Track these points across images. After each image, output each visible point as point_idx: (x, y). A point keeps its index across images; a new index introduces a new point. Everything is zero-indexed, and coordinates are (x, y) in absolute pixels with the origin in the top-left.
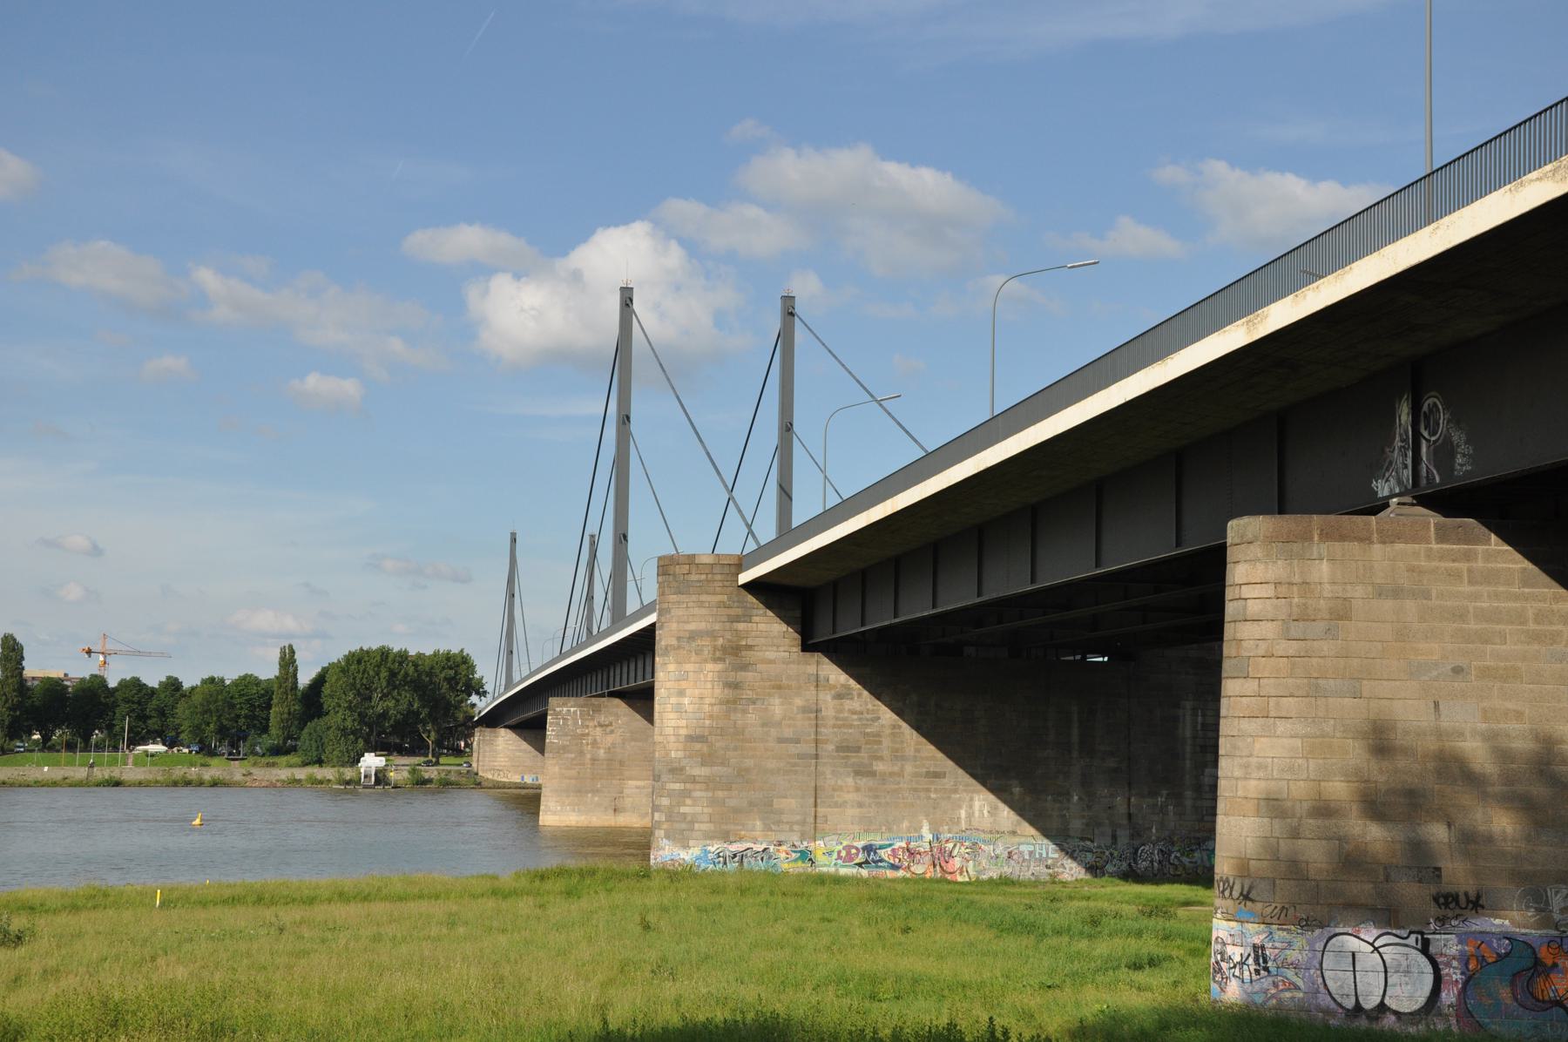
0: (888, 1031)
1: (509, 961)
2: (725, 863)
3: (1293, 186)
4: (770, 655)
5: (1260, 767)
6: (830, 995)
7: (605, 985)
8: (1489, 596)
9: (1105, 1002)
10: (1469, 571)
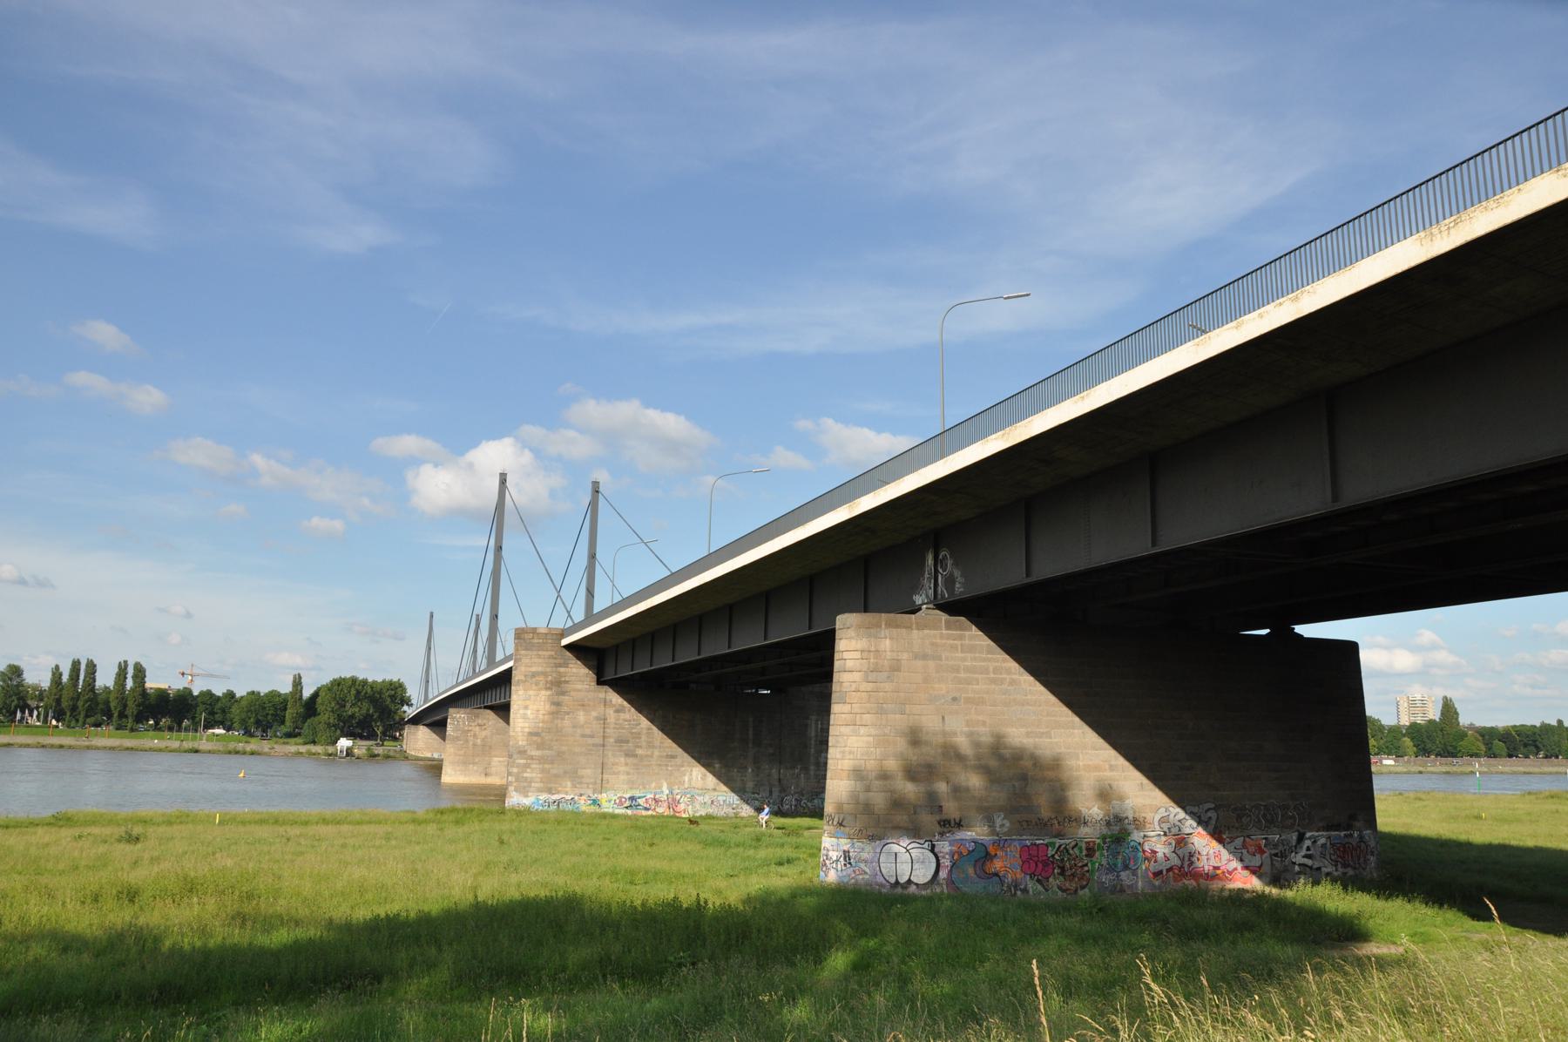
0: (639, 902)
1: (421, 861)
2: (549, 806)
3: (867, 433)
4: (579, 686)
5: (850, 753)
6: (607, 881)
7: (476, 876)
8: (971, 659)
9: (762, 883)
10: (962, 645)
